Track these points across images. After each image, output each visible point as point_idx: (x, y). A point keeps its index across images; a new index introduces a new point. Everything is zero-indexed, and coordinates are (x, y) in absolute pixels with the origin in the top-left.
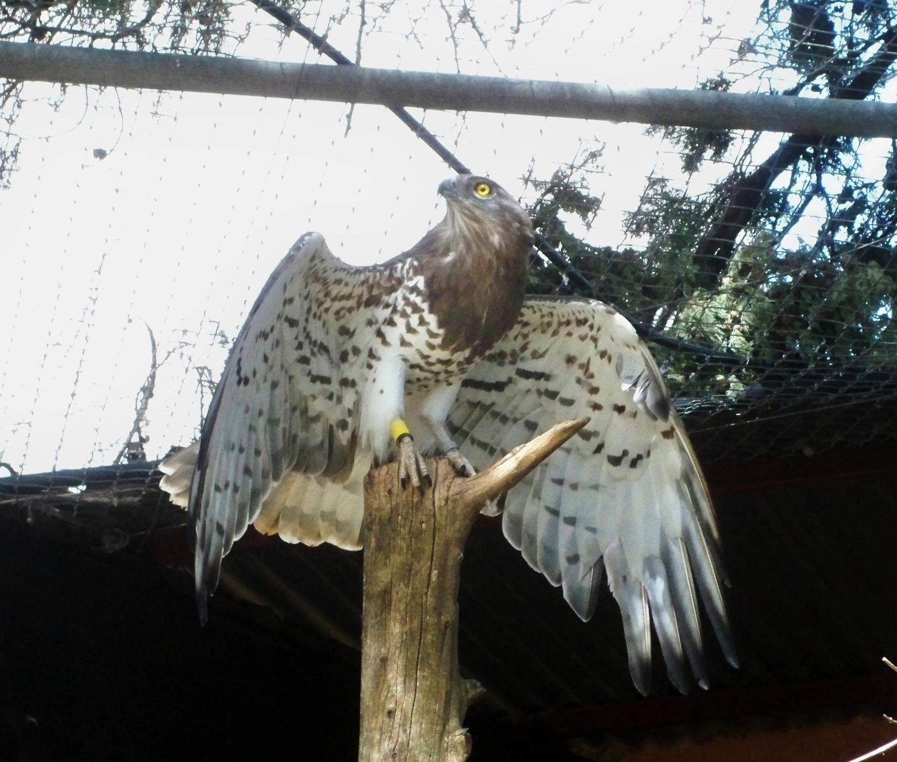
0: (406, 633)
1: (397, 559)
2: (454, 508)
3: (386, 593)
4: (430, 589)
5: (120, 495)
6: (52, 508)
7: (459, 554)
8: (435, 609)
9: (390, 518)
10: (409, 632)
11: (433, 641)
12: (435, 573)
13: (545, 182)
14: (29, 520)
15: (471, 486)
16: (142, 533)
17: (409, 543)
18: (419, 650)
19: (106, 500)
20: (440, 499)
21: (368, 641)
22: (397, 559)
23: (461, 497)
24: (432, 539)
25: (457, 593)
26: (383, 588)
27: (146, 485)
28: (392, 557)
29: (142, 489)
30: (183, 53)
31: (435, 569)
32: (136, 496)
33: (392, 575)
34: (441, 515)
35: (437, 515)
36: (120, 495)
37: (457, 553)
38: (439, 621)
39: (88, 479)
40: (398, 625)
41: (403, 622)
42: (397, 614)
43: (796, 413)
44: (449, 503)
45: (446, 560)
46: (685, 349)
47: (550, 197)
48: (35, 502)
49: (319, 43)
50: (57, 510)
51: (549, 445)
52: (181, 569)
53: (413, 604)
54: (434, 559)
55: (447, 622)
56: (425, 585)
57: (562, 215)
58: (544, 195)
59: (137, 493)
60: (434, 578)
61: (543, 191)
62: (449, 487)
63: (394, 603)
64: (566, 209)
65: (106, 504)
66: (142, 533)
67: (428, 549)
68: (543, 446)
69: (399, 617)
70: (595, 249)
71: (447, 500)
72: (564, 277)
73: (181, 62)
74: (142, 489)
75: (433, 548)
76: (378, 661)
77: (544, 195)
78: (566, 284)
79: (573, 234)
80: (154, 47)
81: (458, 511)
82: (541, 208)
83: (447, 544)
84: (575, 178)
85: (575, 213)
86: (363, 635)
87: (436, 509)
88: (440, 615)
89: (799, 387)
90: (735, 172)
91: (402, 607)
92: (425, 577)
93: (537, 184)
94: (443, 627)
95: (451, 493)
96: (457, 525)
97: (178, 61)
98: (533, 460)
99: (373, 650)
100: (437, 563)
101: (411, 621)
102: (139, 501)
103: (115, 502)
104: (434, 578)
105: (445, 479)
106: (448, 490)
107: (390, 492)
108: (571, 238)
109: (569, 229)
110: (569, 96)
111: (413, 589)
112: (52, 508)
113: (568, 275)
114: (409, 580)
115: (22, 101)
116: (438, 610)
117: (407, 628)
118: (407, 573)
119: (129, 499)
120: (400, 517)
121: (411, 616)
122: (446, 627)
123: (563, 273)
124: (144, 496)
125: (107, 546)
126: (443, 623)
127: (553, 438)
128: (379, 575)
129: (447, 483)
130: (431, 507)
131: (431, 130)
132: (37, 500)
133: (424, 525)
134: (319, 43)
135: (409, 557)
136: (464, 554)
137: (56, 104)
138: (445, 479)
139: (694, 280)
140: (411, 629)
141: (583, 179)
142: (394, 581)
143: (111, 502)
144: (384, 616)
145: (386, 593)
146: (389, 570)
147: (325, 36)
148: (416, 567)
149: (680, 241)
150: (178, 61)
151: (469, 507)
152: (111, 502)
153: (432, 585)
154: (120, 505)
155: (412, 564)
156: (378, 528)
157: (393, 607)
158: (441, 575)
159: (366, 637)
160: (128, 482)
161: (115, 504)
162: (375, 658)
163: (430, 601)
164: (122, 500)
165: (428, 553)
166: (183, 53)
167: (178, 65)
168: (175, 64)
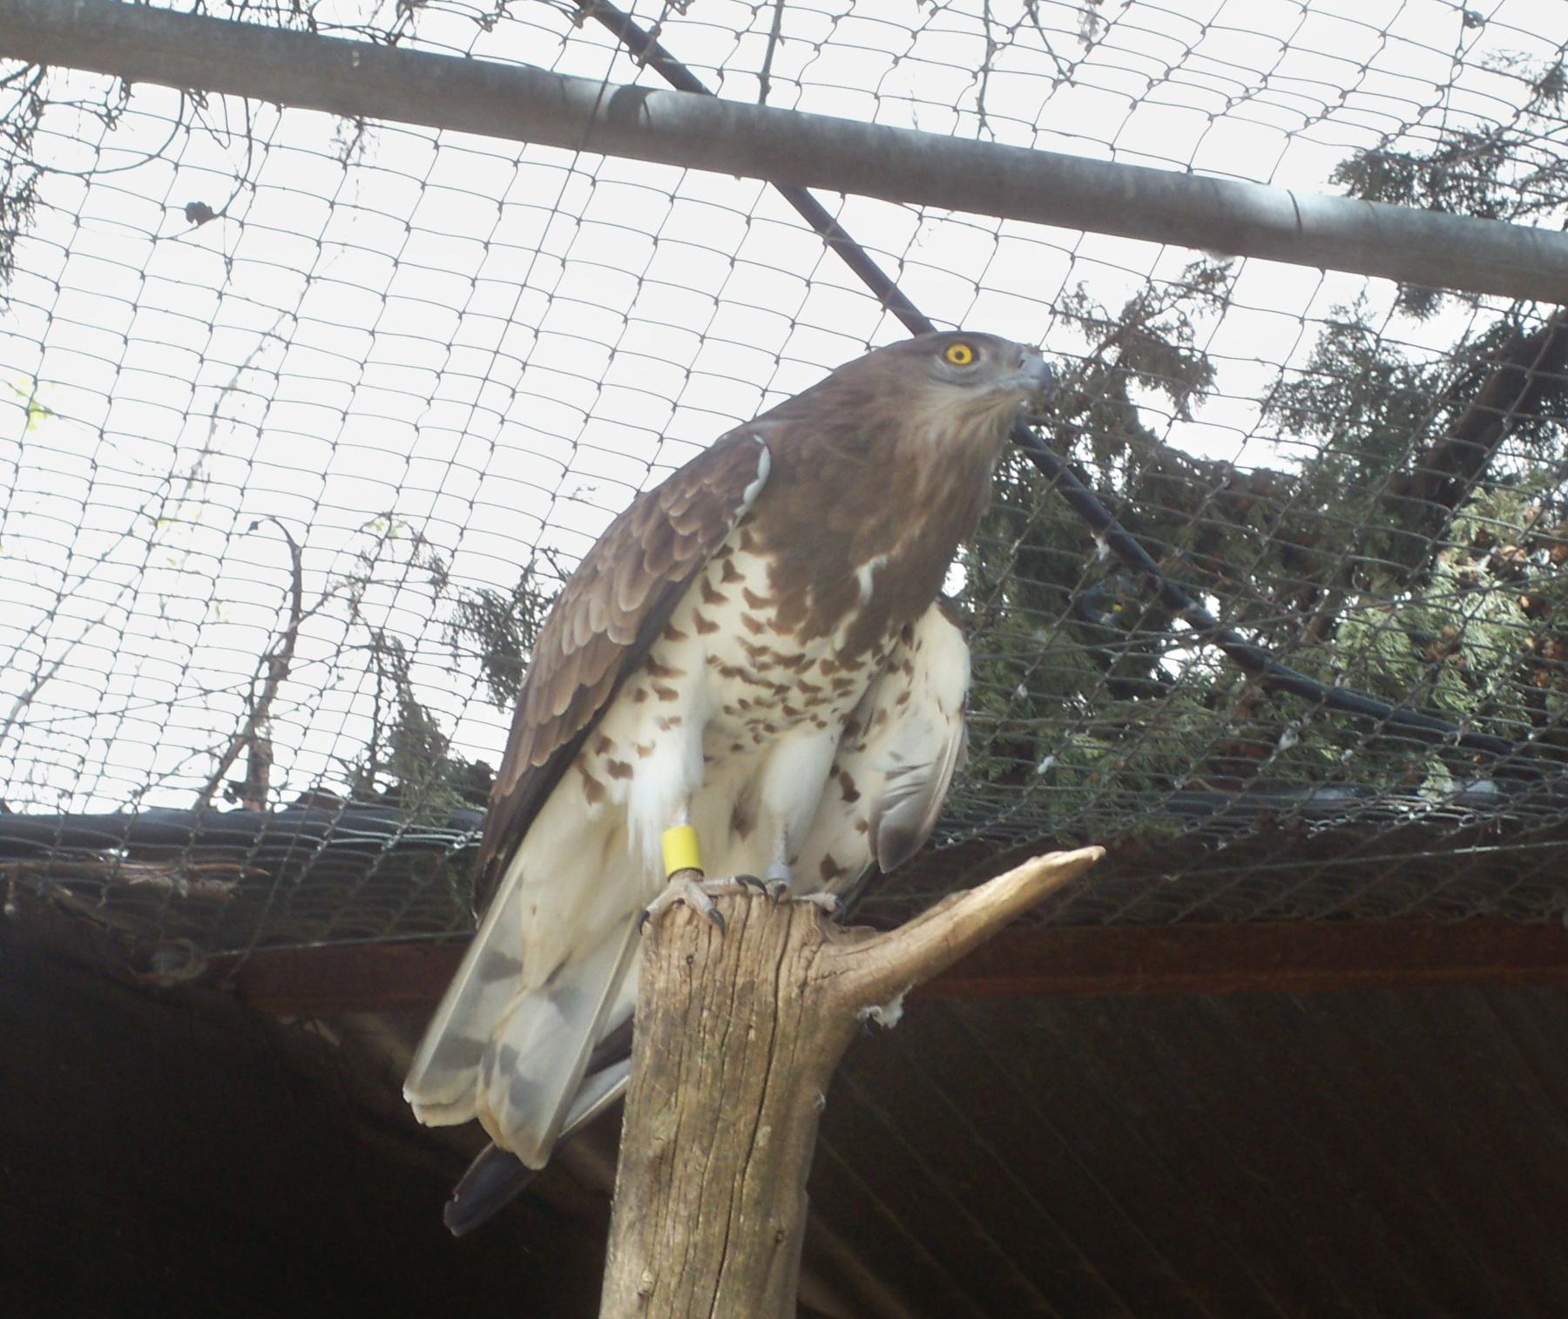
0: (695, 1246)
1: (689, 1095)
2: (815, 1003)
3: (663, 1162)
4: (751, 1163)
5: (193, 876)
6: (59, 888)
7: (817, 1098)
8: (757, 1202)
9: (686, 1013)
10: (700, 1245)
11: (747, 1268)
12: (764, 1131)
13: (1109, 323)
14: (9, 908)
15: (853, 964)
16: (234, 952)
17: (718, 1066)
18: (718, 1282)
19: (167, 882)
20: (789, 984)
21: (619, 1255)
22: (689, 1095)
23: (831, 983)
24: (765, 1065)
25: (806, 1175)
26: (658, 1151)
27: (248, 861)
28: (681, 1089)
29: (239, 867)
30: (370, 40)
31: (767, 1124)
32: (226, 879)
33: (678, 1127)
34: (787, 1015)
35: (781, 1014)
36: (193, 876)
37: (812, 1096)
38: (764, 1229)
39: (131, 839)
40: (680, 1228)
41: (692, 1224)
42: (682, 1205)
43: (1559, 843)
44: (807, 991)
45: (789, 1108)
46: (1337, 701)
47: (1111, 355)
48: (23, 873)
49: (642, 45)
50: (68, 892)
51: (1017, 895)
52: (309, 1026)
53: (715, 1189)
54: (766, 1102)
55: (780, 1232)
56: (743, 1155)
57: (1135, 391)
58: (1101, 348)
59: (226, 876)
60: (762, 1139)
61: (1103, 339)
62: (810, 963)
63: (676, 1183)
64: (1145, 382)
65: (166, 889)
66: (234, 952)
67: (755, 1081)
68: (1005, 897)
69: (684, 1213)
70: (1196, 464)
71: (803, 985)
72: (1100, 543)
73: (361, 58)
74: (239, 867)
75: (766, 1080)
76: (635, 1296)
77: (1101, 348)
78: (1101, 557)
79: (1153, 431)
80: (312, 23)
81: (823, 1012)
82: (1095, 372)
83: (794, 1079)
84: (1164, 317)
85: (1161, 391)
86: (611, 1241)
87: (780, 1004)
88: (767, 1215)
89: (1561, 796)
90: (1504, 323)
91: (693, 1194)
92: (744, 1139)
93: (1090, 324)
94: (770, 1242)
95: (812, 973)
96: (819, 1038)
97: (355, 54)
98: (981, 924)
99: (625, 1276)
100: (771, 1112)
101: (708, 1223)
102: (231, 891)
103: (184, 888)
104: (762, 1139)
105: (804, 944)
106: (808, 967)
107: (690, 959)
108: (1150, 438)
109: (1146, 420)
110: (1131, 193)
111: (717, 1159)
112: (59, 888)
113: (1112, 541)
114: (712, 1140)
115: (43, 103)
116: (765, 1204)
117: (697, 1237)
118: (709, 1124)
119: (214, 884)
120: (705, 1013)
121: (707, 1215)
122: (777, 1241)
123: (1098, 534)
124: (242, 882)
125: (162, 972)
126: (772, 1233)
127: (1025, 884)
128: (655, 1124)
129: (806, 953)
130: (772, 1000)
131: (857, 234)
132: (29, 869)
133: (752, 1034)
134: (642, 45)
135: (717, 1095)
136: (827, 1099)
137: (109, 115)
138: (804, 944)
139: (1386, 545)
140: (705, 1239)
141: (1185, 323)
142: (681, 1141)
143: (175, 887)
144: (654, 1207)
145: (663, 1162)
146: (675, 1117)
147: (657, 31)
148: (728, 1114)
149: (1375, 450)
150: (355, 54)
151: (846, 1004)
152: (175, 887)
153: (756, 1154)
154: (192, 896)
155: (720, 1110)
156: (660, 1029)
157: (674, 1192)
158: (777, 1137)
159: (616, 1246)
160: (210, 852)
161: (184, 893)
162: (628, 1289)
163: (749, 1187)
164: (199, 885)
165: (755, 1092)
166: (370, 40)
167: (356, 64)
168: (350, 59)
